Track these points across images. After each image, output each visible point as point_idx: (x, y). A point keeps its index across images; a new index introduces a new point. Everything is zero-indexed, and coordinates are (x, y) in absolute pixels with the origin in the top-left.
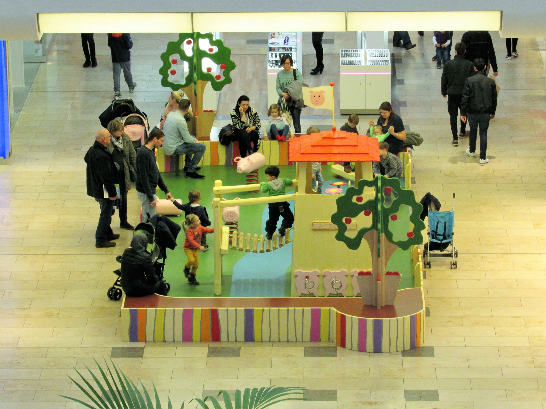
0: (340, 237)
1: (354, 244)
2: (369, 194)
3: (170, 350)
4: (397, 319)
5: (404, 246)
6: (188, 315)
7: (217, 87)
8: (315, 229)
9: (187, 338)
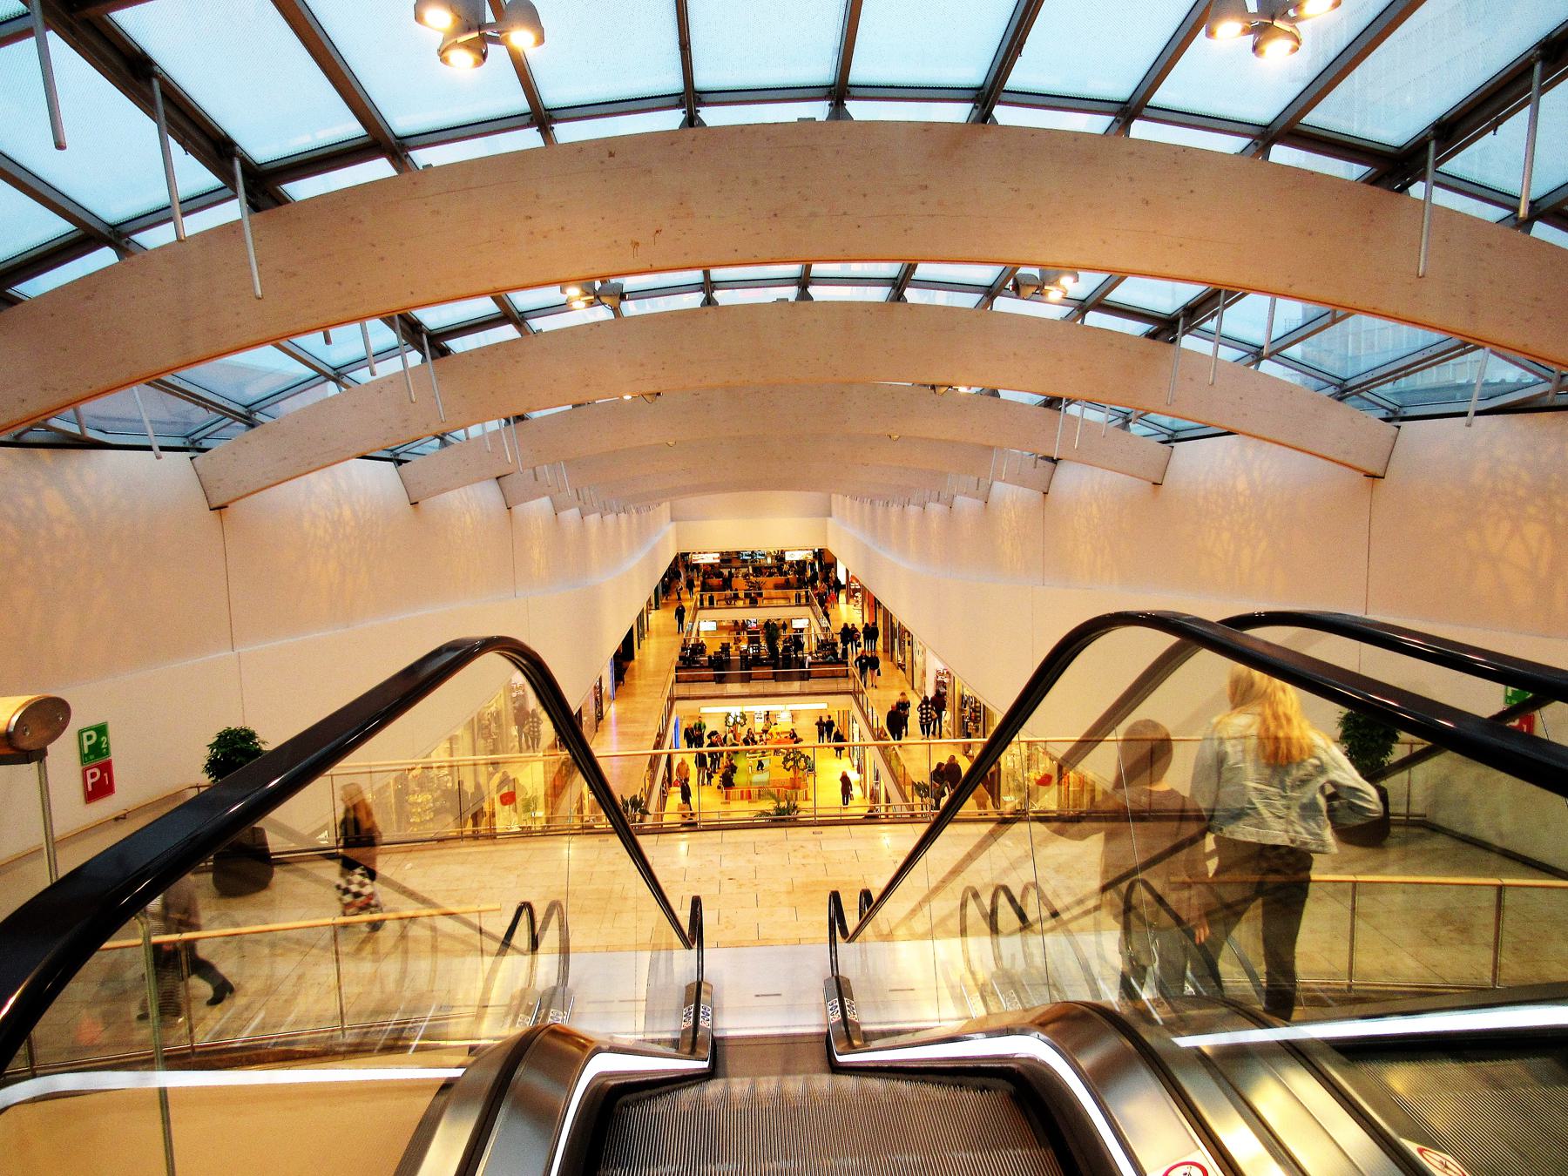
0: (785, 768)
1: (788, 770)
2: (792, 756)
3: (737, 802)
4: (451, 755)
5: (803, 770)
6: (742, 792)
7: (742, 726)
8: (777, 766)
9: (742, 798)
